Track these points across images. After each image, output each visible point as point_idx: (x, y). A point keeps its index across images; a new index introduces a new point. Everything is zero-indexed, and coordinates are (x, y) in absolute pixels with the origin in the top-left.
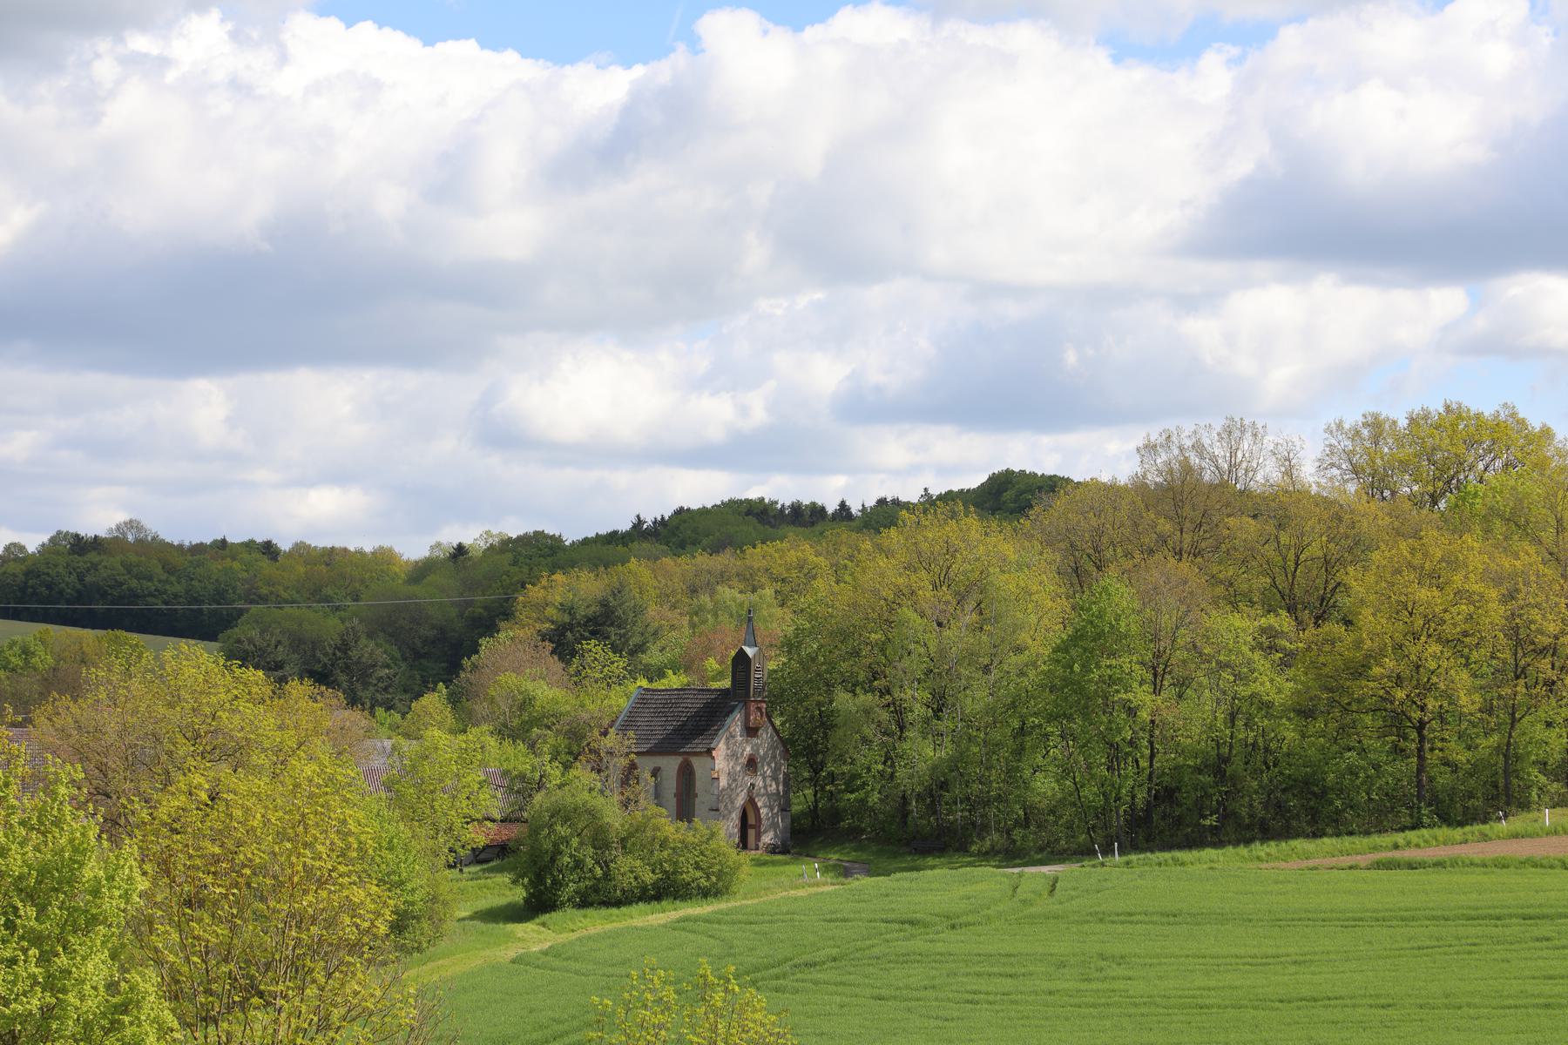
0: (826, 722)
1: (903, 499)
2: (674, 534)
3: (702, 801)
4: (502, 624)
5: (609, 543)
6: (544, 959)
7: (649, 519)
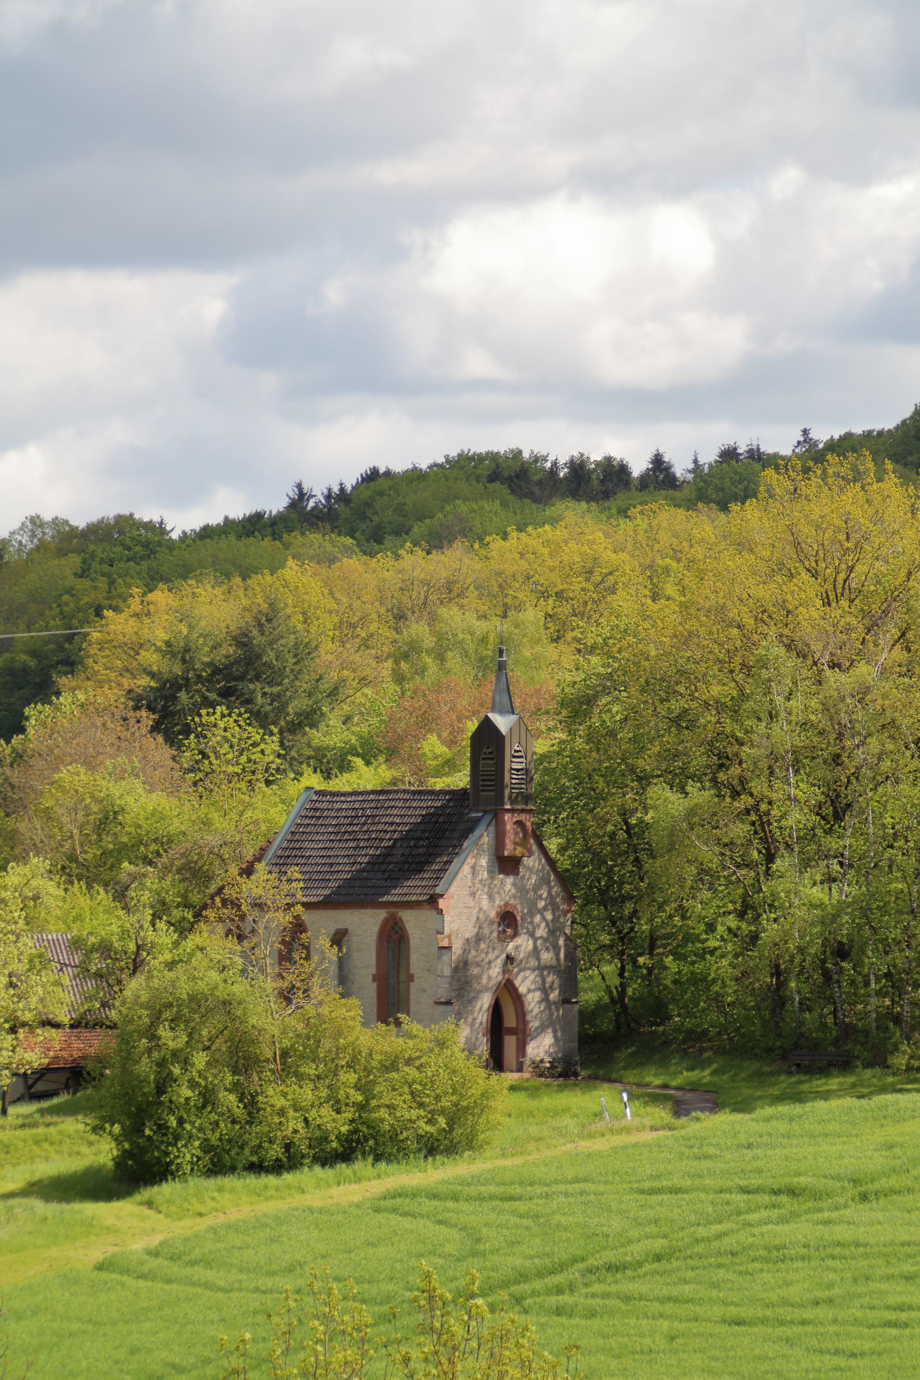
0: (634, 841)
1: (768, 448)
2: (363, 517)
3: (427, 981)
4: (63, 681)
5: (249, 533)
6: (153, 1263)
7: (318, 489)
